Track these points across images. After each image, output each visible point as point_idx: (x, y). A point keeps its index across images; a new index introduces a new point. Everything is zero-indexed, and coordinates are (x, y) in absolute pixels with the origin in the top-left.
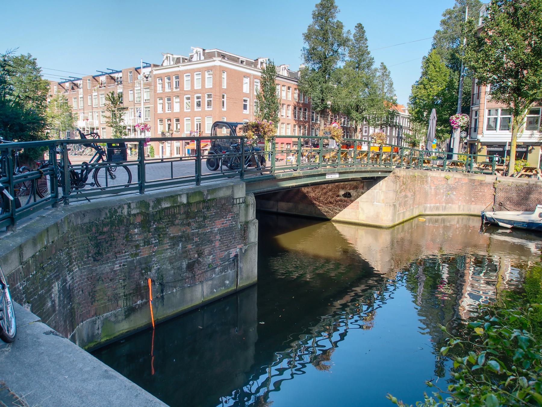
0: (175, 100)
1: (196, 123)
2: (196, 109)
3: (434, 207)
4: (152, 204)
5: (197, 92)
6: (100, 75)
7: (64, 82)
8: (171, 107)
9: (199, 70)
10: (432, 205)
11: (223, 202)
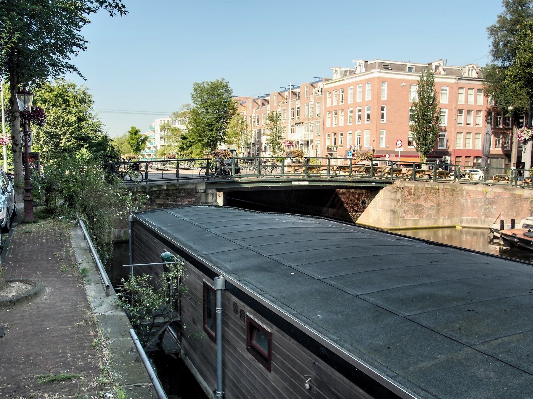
0: (340, 113)
1: (356, 137)
2: (358, 123)
3: (471, 220)
4: (148, 188)
5: (358, 105)
6: (318, 82)
7: (284, 91)
8: (337, 122)
9: (360, 82)
10: (469, 218)
11: (189, 191)
